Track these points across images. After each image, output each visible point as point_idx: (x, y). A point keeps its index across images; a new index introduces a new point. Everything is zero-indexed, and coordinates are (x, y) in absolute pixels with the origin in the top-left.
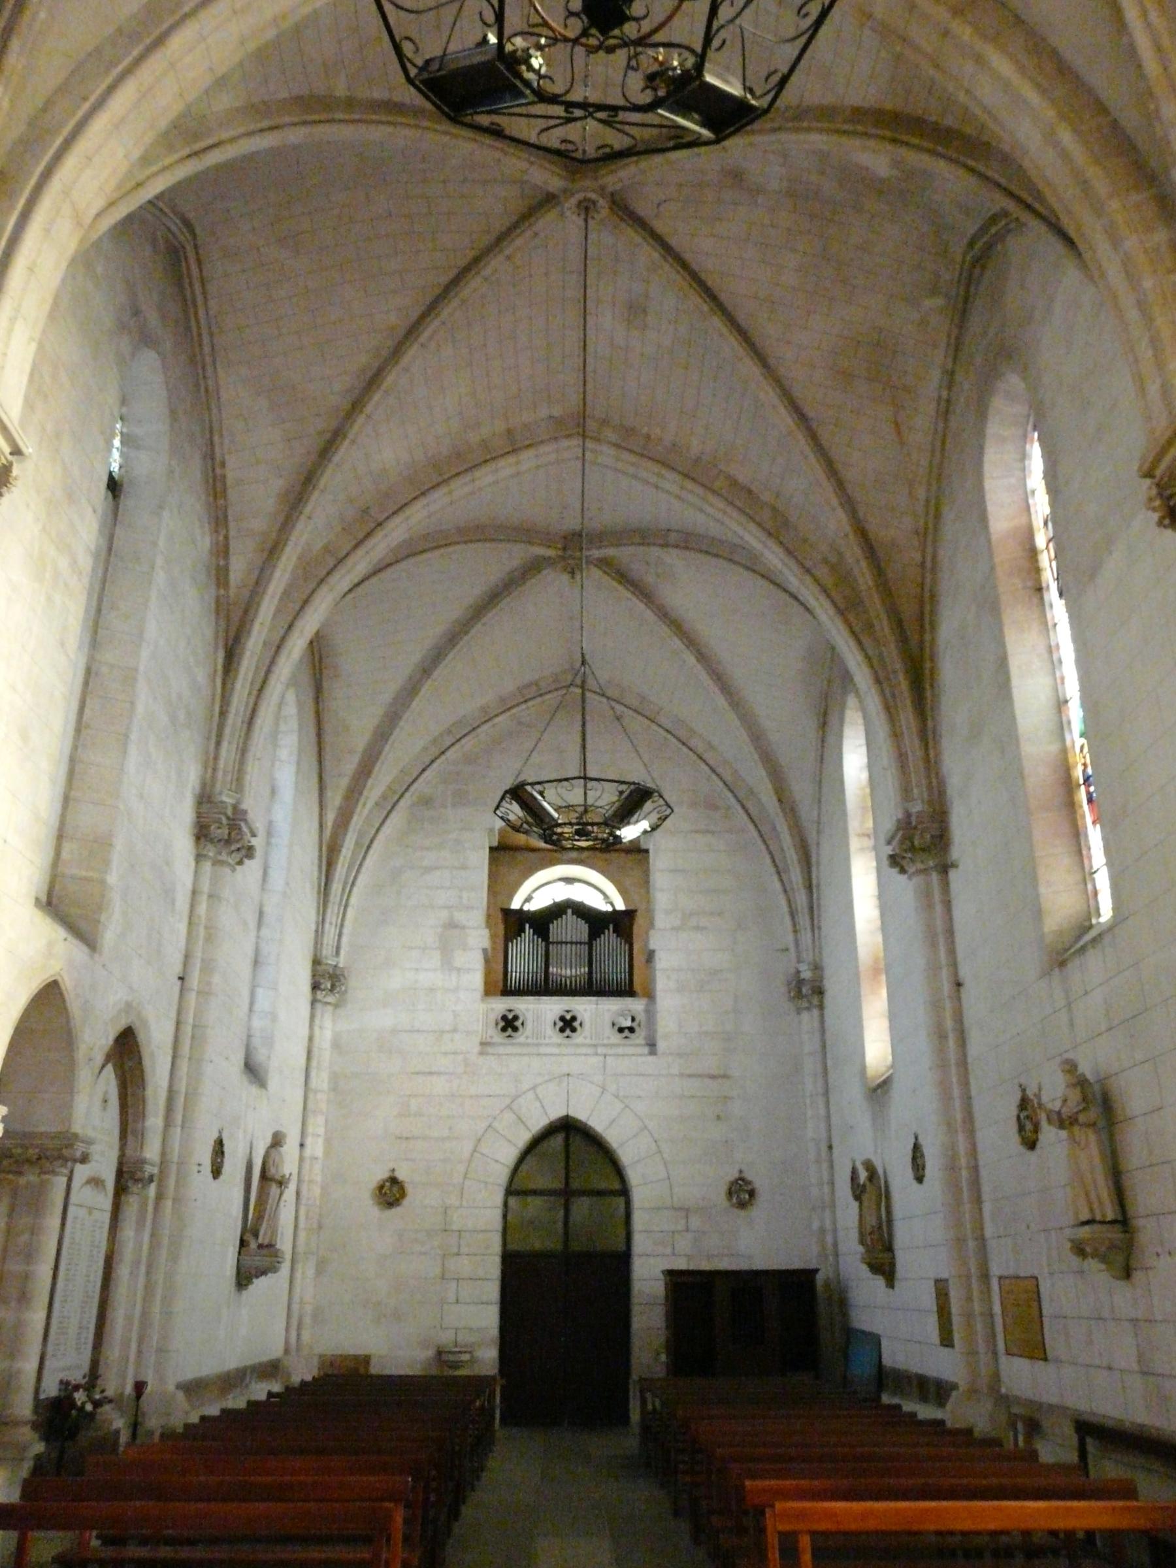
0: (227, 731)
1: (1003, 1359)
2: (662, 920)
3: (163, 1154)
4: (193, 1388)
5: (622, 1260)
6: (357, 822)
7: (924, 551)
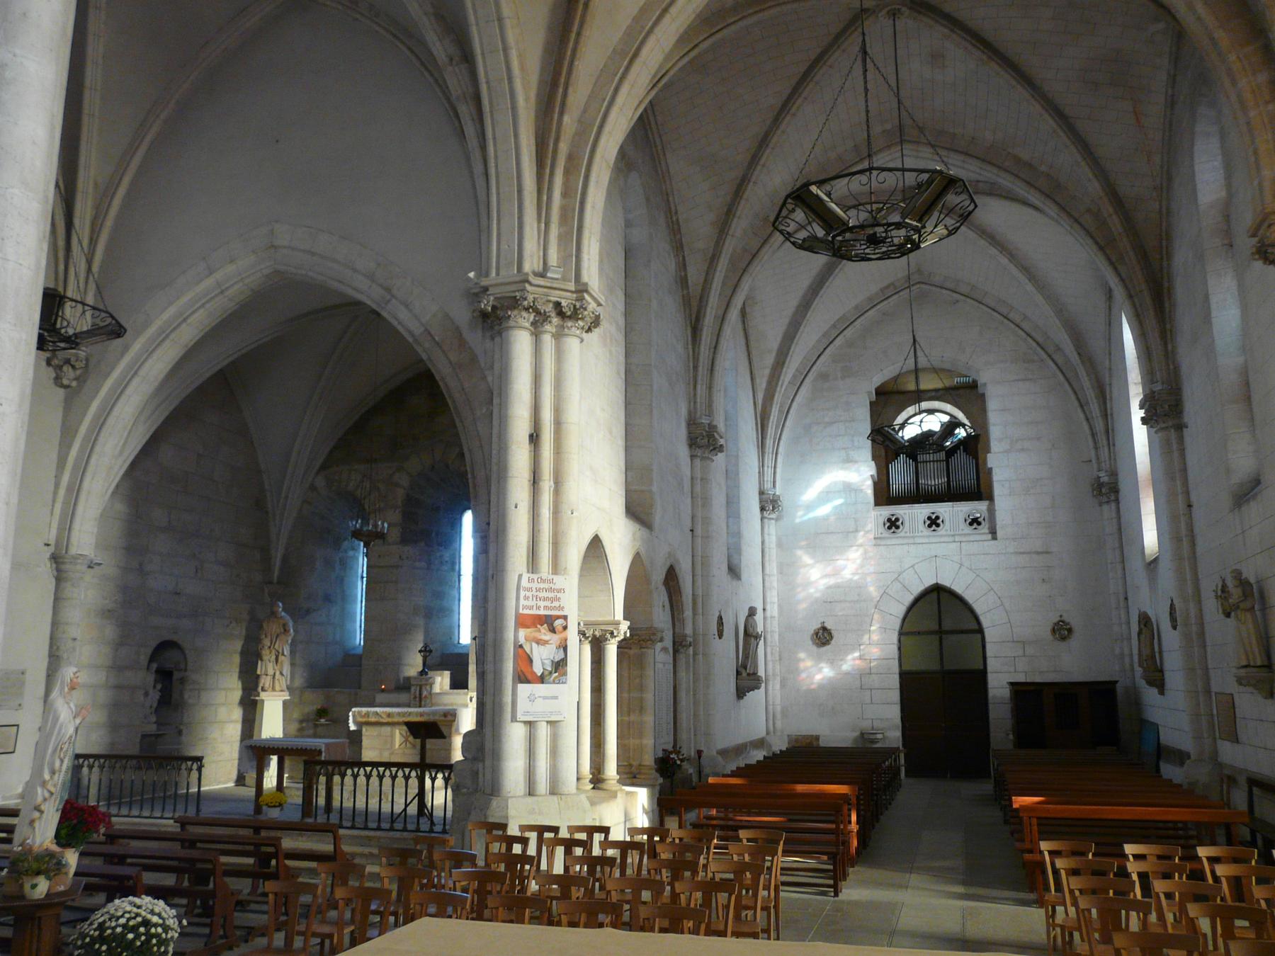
0: (699, 378)
1: (1219, 742)
2: (995, 446)
3: (694, 630)
4: (723, 753)
5: (981, 676)
6: (778, 398)
7: (1161, 201)
